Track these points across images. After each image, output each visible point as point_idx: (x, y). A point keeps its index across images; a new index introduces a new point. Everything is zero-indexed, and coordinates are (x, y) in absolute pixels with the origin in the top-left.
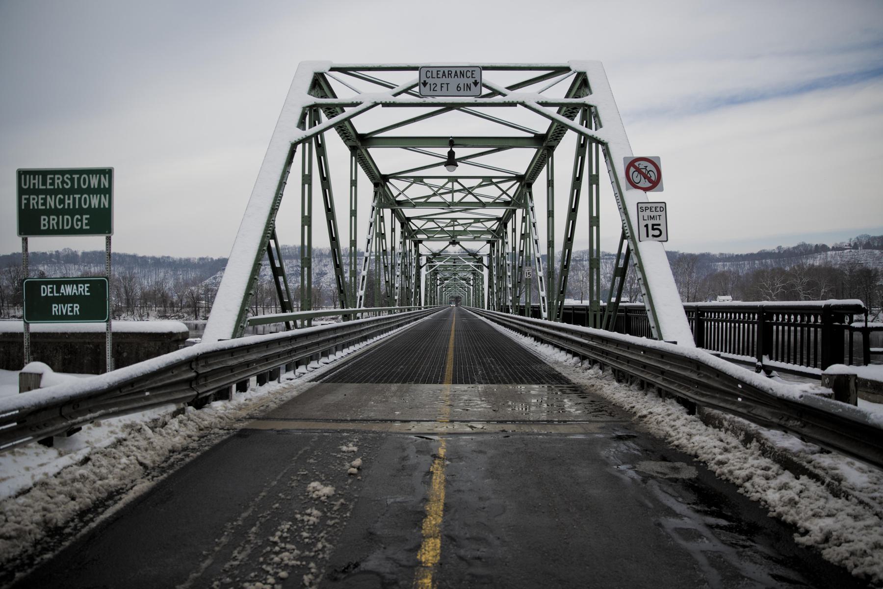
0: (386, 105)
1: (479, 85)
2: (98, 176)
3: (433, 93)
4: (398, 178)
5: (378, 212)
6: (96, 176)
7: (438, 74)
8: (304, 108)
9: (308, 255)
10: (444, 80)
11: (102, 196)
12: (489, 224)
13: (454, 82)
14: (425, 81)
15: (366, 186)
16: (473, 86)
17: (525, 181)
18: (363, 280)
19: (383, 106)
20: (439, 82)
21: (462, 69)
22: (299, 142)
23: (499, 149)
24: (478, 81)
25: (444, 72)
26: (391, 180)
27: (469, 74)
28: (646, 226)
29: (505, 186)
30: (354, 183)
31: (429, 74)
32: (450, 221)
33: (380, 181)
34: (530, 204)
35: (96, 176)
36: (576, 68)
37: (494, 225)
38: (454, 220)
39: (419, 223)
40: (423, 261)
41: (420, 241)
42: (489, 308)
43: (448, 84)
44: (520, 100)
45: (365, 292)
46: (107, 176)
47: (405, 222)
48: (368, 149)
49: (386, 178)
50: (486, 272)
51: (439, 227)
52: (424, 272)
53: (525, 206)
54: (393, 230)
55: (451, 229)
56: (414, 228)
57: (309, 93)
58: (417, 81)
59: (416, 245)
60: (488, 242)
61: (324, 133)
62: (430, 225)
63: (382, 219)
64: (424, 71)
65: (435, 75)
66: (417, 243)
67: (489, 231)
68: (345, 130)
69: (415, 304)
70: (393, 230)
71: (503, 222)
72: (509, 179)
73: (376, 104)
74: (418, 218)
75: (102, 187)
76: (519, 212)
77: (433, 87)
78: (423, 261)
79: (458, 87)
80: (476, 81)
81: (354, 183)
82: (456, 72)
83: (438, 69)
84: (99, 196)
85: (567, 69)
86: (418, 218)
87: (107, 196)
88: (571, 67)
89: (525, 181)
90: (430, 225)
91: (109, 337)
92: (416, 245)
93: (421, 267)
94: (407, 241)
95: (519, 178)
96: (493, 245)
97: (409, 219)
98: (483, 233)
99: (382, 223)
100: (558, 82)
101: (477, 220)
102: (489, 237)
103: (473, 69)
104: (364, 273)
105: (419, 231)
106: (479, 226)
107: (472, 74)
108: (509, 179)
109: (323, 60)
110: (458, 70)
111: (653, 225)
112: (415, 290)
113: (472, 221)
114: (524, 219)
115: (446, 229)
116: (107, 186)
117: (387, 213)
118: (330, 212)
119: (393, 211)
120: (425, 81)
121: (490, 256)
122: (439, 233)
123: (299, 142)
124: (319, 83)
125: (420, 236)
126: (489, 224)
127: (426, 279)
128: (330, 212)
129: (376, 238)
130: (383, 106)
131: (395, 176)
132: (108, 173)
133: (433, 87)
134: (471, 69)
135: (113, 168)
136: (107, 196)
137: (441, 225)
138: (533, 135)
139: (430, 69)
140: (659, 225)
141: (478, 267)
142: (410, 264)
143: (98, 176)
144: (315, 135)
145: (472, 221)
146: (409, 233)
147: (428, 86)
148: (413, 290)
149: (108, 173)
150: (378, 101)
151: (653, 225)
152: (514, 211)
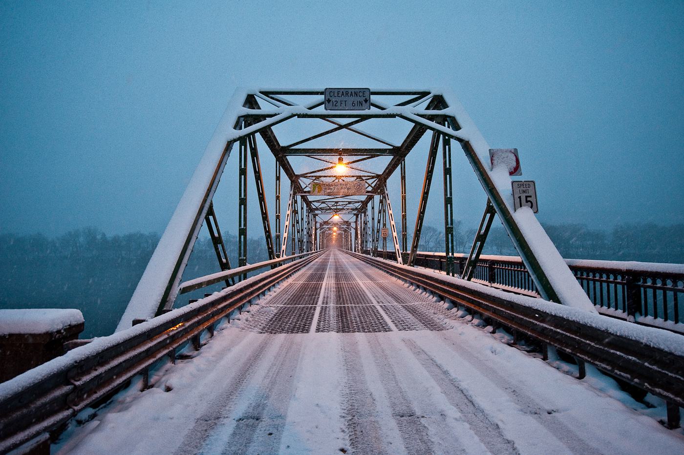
4: (305, 177)
5: (294, 198)
7: (338, 94)
8: (239, 118)
10: (343, 98)
12: (357, 205)
13: (351, 99)
14: (329, 99)
15: (285, 180)
16: (364, 102)
17: (382, 179)
18: (285, 239)
19: (298, 117)
20: (337, 99)
21: (356, 91)
22: (235, 140)
23: (373, 157)
26: (301, 178)
28: (520, 197)
29: (370, 181)
30: (278, 178)
31: (331, 94)
32: (334, 203)
33: (294, 178)
34: (386, 192)
36: (434, 92)
37: (358, 205)
38: (337, 202)
39: (317, 204)
40: (318, 225)
42: (355, 251)
43: (345, 101)
44: (399, 113)
47: (309, 203)
52: (318, 231)
53: (382, 193)
54: (302, 208)
55: (335, 207)
56: (314, 207)
57: (244, 106)
58: (324, 100)
59: (315, 217)
60: (354, 214)
61: (256, 134)
62: (323, 205)
63: (296, 202)
64: (327, 93)
65: (336, 94)
66: (315, 216)
67: (356, 209)
68: (271, 141)
69: (314, 250)
70: (302, 208)
71: (365, 204)
72: (373, 177)
73: (293, 116)
74: (318, 201)
76: (377, 198)
78: (318, 225)
79: (353, 103)
80: (366, 99)
81: (278, 178)
82: (352, 93)
83: (339, 90)
88: (431, 91)
90: (323, 205)
92: (315, 217)
93: (317, 229)
94: (310, 215)
95: (378, 176)
96: (357, 217)
97: (311, 202)
99: (296, 204)
100: (374, 139)
101: (350, 203)
102: (355, 212)
103: (364, 90)
105: (317, 209)
106: (351, 206)
108: (373, 177)
109: (254, 88)
110: (353, 91)
112: (315, 242)
113: (347, 203)
114: (381, 202)
115: (332, 207)
117: (299, 198)
119: (302, 197)
120: (329, 99)
121: (356, 222)
123: (235, 140)
124: (251, 101)
125: (316, 212)
126: (357, 205)
130: (298, 117)
134: (362, 91)
137: (330, 205)
139: (333, 91)
140: (530, 197)
142: (312, 228)
144: (248, 135)
145: (347, 203)
146: (311, 210)
147: (331, 102)
148: (313, 242)
150: (295, 113)
151: (527, 197)
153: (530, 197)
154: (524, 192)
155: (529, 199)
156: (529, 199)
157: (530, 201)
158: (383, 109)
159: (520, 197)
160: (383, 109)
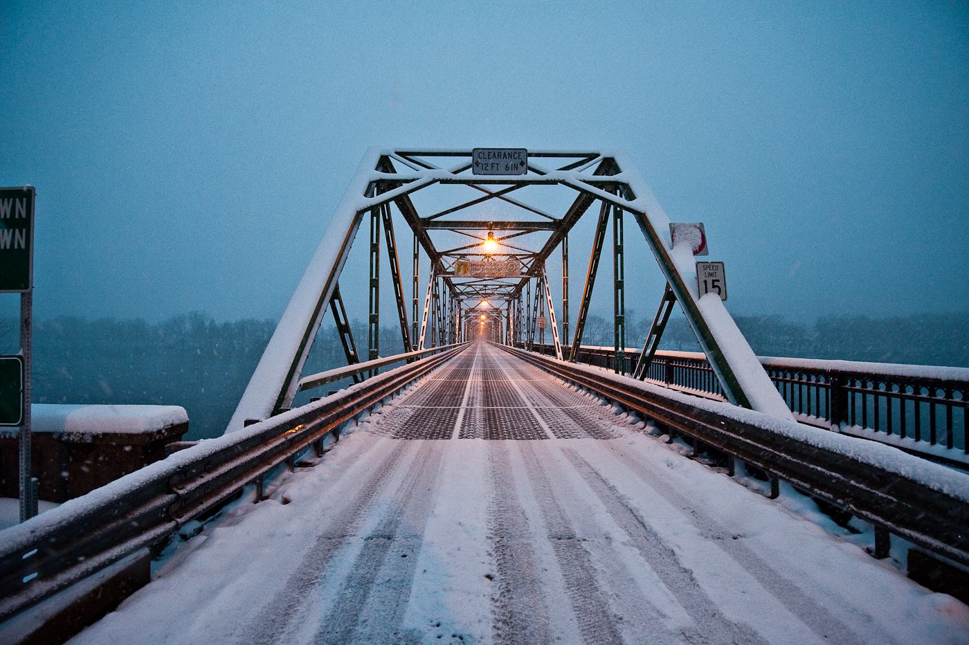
0: (443, 181)
1: (525, 166)
2: (11, 200)
3: (484, 172)
5: (434, 280)
6: (9, 201)
8: (371, 183)
9: (376, 312)
11: (17, 230)
12: (509, 289)
13: (503, 162)
17: (540, 258)
19: (441, 183)
24: (524, 161)
25: (494, 153)
27: (516, 156)
28: (705, 282)
29: (525, 261)
30: (416, 256)
33: (435, 256)
35: (9, 201)
36: (605, 154)
37: (511, 290)
38: (485, 286)
39: (462, 288)
40: (463, 313)
41: (462, 300)
44: (561, 179)
45: (423, 310)
46: (25, 199)
47: (452, 286)
48: (427, 231)
49: (440, 254)
50: (504, 321)
51: (476, 290)
52: (463, 320)
54: (444, 292)
55: (484, 292)
56: (458, 291)
60: (507, 300)
62: (469, 289)
63: (437, 284)
64: (476, 154)
66: (460, 301)
67: (509, 294)
70: (444, 292)
71: (519, 288)
72: (530, 256)
73: (434, 181)
74: (462, 284)
75: (17, 217)
77: (484, 166)
78: (463, 313)
81: (416, 256)
83: (490, 151)
84: (11, 230)
85: (598, 155)
86: (462, 284)
87: (24, 230)
88: (600, 153)
89: (540, 258)
90: (469, 289)
91: (23, 449)
95: (534, 255)
97: (455, 285)
98: (505, 295)
101: (501, 286)
104: (424, 324)
105: (462, 293)
106: (503, 290)
107: (519, 156)
108: (530, 256)
109: (389, 148)
111: (714, 281)
116: (24, 216)
117: (440, 280)
118: (396, 279)
121: (508, 310)
122: (475, 294)
124: (384, 163)
125: (461, 297)
126: (509, 289)
127: (465, 325)
128: (396, 279)
129: (145, 544)
130: (441, 183)
131: (446, 253)
132: (27, 196)
133: (484, 166)
134: (498, 151)
135: (34, 188)
136: (24, 230)
138: (552, 221)
140: (718, 281)
141: (498, 317)
143: (11, 200)
144: (382, 204)
146: (454, 295)
149: (27, 196)
151: (714, 281)
152: (528, 280)
153: (718, 281)
154: (711, 275)
155: (716, 283)
156: (716, 283)
157: (717, 286)
158: (542, 174)
159: (705, 282)
160: (542, 174)
